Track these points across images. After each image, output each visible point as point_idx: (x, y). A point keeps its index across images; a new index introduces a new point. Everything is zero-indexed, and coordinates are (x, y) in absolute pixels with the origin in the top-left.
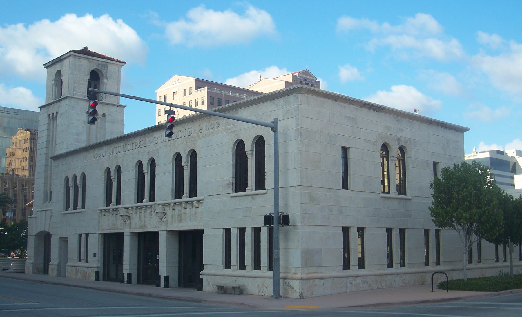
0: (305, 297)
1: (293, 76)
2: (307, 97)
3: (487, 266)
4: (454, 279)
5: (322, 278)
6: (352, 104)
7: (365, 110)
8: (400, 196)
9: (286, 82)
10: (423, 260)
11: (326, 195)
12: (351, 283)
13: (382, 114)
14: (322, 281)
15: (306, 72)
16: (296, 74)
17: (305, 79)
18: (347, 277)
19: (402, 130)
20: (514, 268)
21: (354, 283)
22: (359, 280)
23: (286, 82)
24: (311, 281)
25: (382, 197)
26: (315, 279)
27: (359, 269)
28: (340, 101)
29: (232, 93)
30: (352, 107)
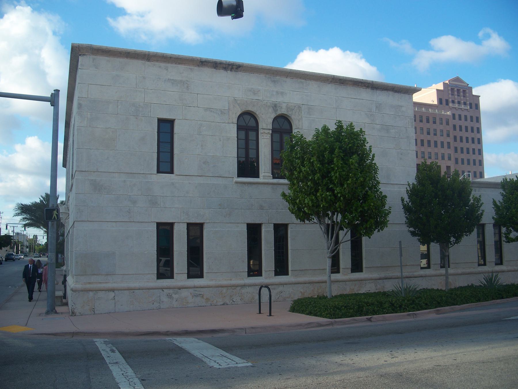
0: (77, 314)
1: (445, 84)
2: (94, 59)
3: (460, 271)
4: (386, 290)
5: (113, 290)
6: (179, 64)
7: (207, 71)
8: (276, 181)
9: (437, 90)
10: (328, 263)
11: (125, 181)
12: (169, 296)
13: (240, 75)
14: (112, 294)
15: (458, 79)
16: (447, 82)
17: (456, 86)
18: (162, 289)
19: (282, 93)
20: (451, 279)
21: (175, 296)
22: (185, 293)
23: (437, 90)
24: (91, 294)
25: (237, 183)
26: (97, 290)
27: (188, 278)
28: (157, 61)
29: (445, 112)
30: (181, 67)
